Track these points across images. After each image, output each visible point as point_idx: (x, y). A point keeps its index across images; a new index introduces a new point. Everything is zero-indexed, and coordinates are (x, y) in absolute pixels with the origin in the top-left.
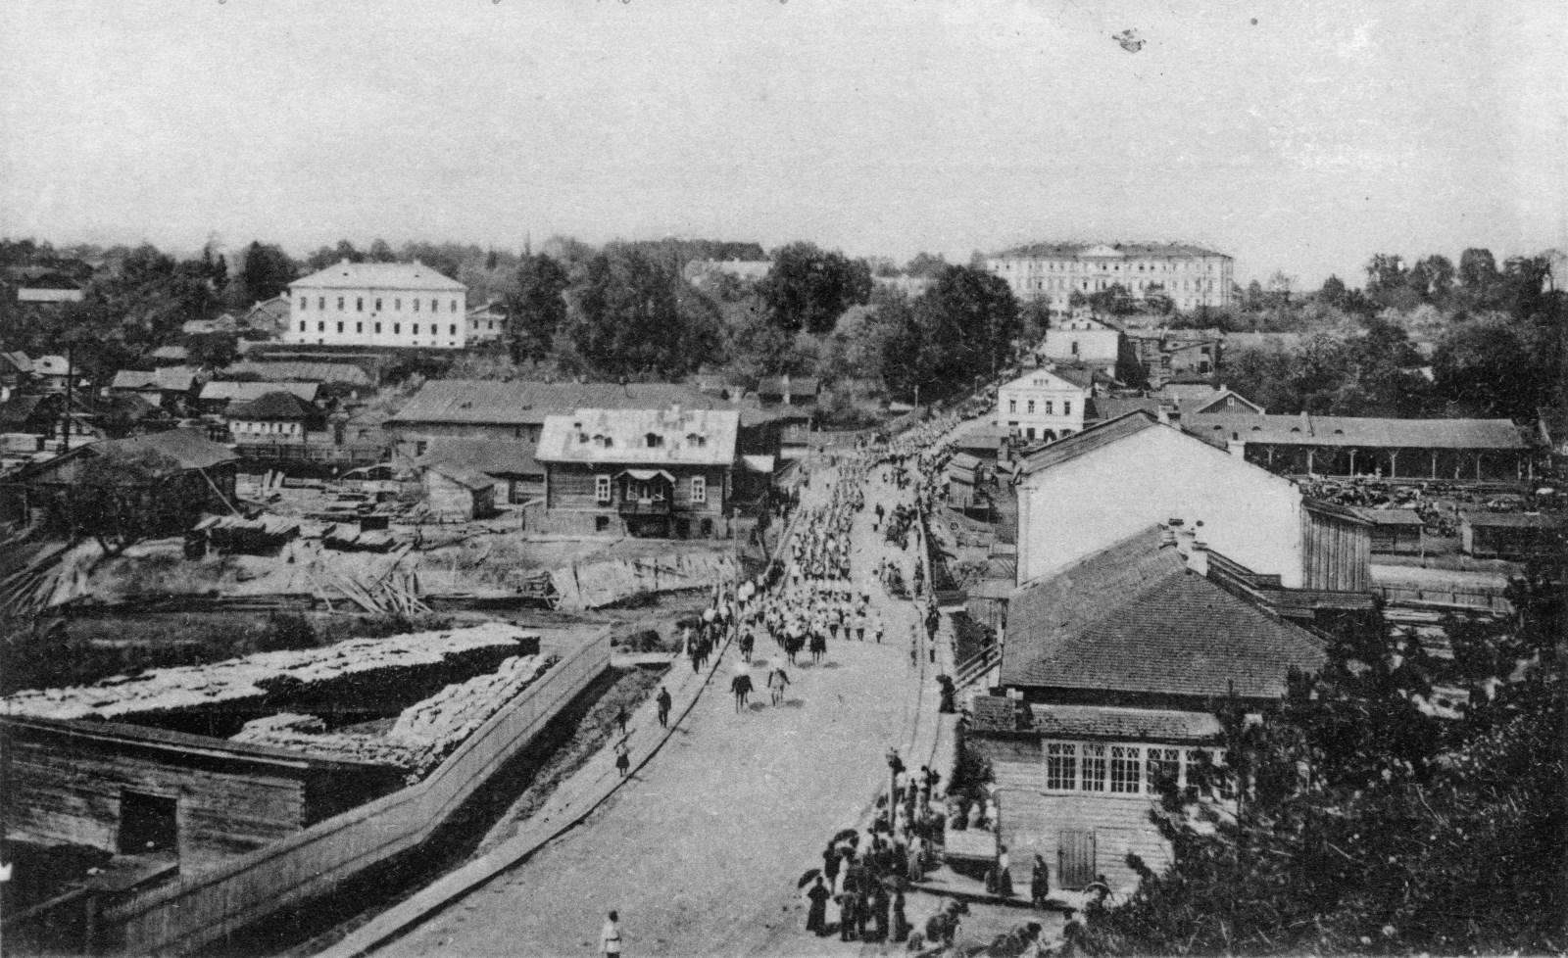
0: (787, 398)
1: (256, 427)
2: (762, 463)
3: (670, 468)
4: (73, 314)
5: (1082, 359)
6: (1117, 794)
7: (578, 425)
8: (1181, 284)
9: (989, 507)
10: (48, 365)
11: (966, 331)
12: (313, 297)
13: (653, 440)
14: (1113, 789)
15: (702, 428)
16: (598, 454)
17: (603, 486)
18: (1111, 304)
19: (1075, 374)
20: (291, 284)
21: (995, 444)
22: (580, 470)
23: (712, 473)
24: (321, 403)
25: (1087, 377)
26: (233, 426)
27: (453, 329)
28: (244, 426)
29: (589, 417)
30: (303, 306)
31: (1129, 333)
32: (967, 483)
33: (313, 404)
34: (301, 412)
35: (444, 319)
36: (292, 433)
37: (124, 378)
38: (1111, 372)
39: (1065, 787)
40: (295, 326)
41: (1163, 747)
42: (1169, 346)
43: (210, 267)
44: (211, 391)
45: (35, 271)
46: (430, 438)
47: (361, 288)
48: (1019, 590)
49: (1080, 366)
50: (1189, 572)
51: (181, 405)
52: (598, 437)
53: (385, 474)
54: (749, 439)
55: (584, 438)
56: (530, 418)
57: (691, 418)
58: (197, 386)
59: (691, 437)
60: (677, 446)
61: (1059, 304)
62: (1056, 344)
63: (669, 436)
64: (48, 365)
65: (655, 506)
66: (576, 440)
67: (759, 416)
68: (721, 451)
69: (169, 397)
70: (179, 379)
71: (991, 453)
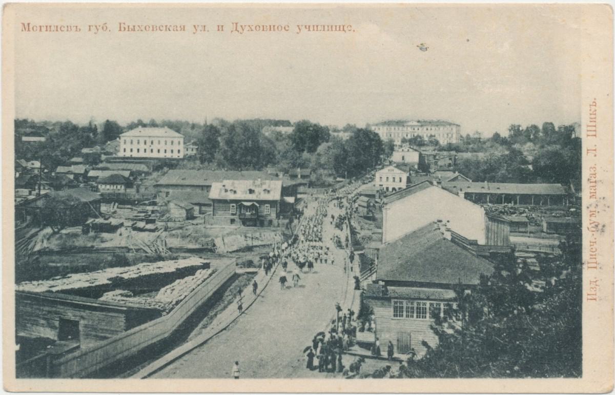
0: (299, 176)
1: (108, 187)
2: (291, 200)
3: (257, 201)
4: (42, 146)
5: (406, 162)
6: (418, 319)
7: (224, 186)
8: (441, 135)
9: (372, 216)
10: (33, 164)
11: (363, 152)
12: (128, 140)
13: (251, 191)
14: (417, 317)
15: (268, 187)
16: (231, 196)
17: (233, 209)
18: (416, 142)
19: (403, 168)
20: (121, 135)
21: (374, 193)
22: (223, 203)
23: (272, 203)
24: (131, 178)
25: (408, 169)
26: (99, 186)
27: (179, 151)
28: (103, 186)
29: (228, 183)
30: (125, 143)
31: (423, 152)
32: (364, 207)
33: (128, 178)
34: (124, 181)
35: (176, 148)
36: (121, 189)
37: (60, 169)
38: (416, 167)
39: (400, 316)
40: (122, 150)
41: (435, 302)
42: (437, 157)
43: (91, 129)
44: (92, 173)
45: (28, 130)
46: (171, 191)
47: (146, 137)
48: (383, 246)
49: (405, 165)
50: (444, 239)
51: (81, 179)
52: (231, 190)
53: (154, 204)
54: (285, 191)
55: (226, 191)
56: (207, 184)
57: (265, 184)
58: (87, 172)
59: (265, 190)
60: (260, 194)
61: (398, 142)
62: (396, 157)
63: (257, 190)
64: (33, 164)
65: (251, 215)
66: (223, 191)
67: (289, 183)
68: (276, 195)
69: (77, 176)
70: (80, 169)
71: (374, 196)
